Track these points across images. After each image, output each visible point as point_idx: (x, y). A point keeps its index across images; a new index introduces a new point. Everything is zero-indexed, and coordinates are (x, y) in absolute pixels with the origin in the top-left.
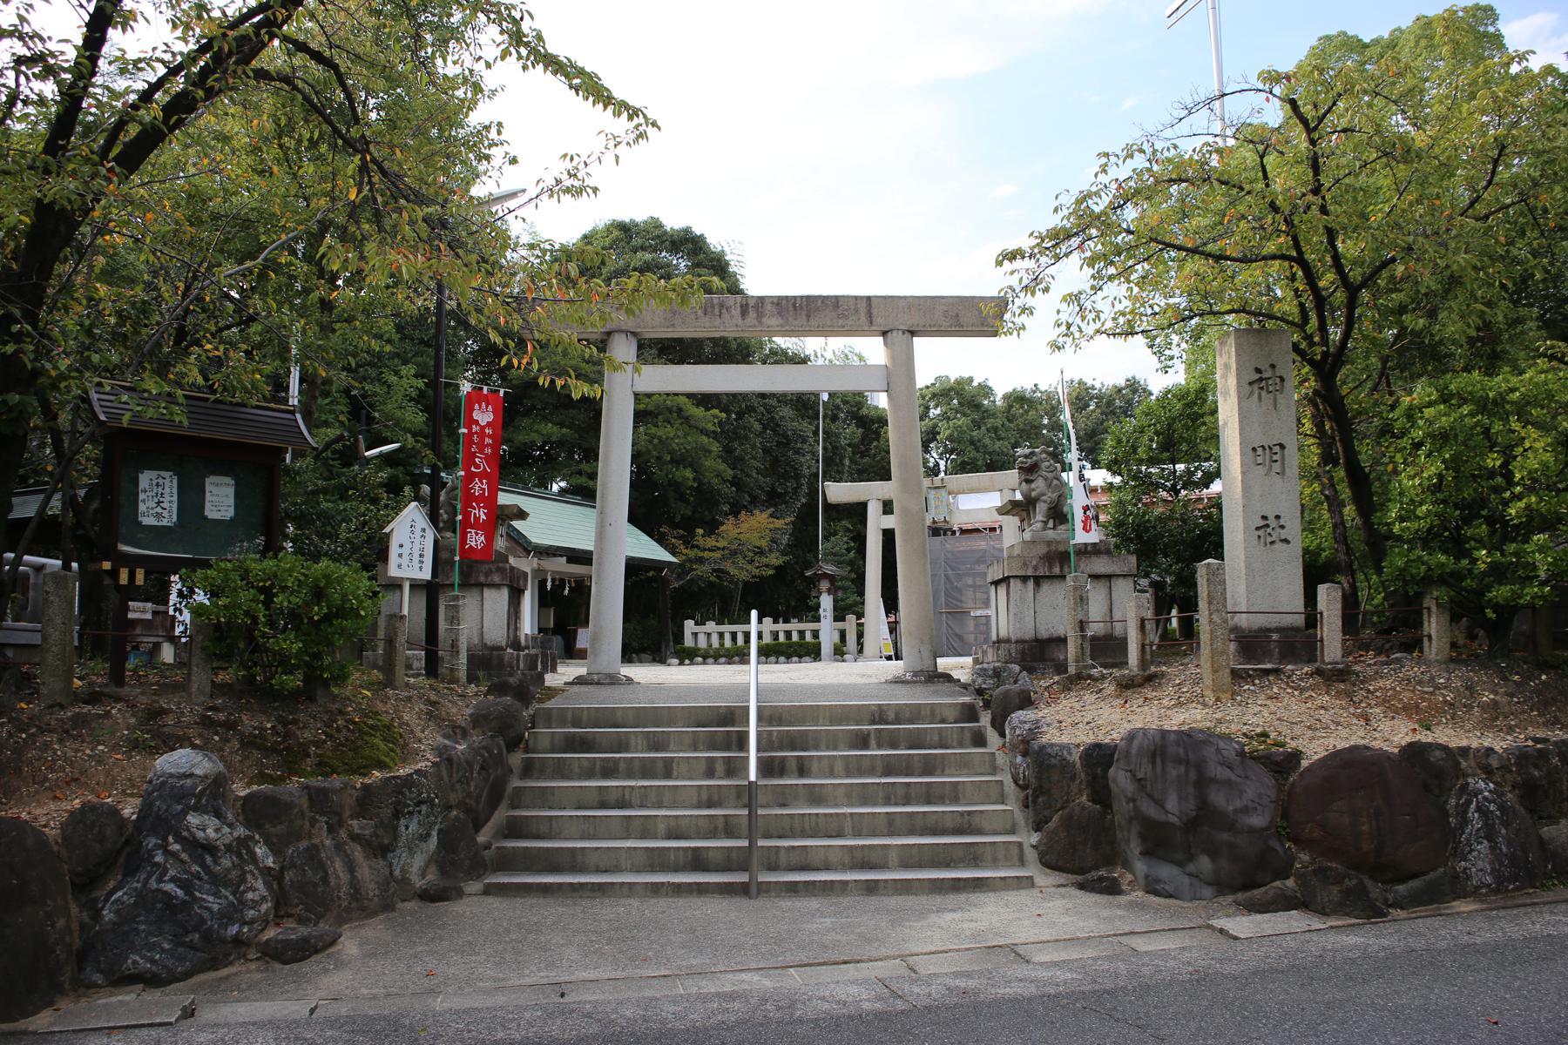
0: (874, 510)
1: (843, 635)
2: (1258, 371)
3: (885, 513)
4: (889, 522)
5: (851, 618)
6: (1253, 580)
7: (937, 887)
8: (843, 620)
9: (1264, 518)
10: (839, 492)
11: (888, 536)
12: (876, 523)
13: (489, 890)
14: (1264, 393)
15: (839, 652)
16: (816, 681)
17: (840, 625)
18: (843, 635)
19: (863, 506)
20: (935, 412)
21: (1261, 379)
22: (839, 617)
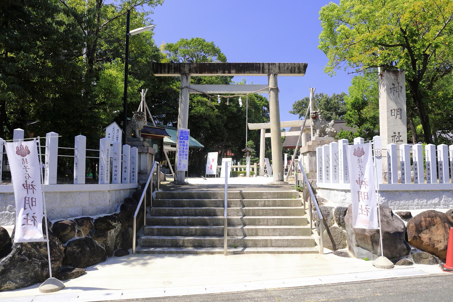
0: (262, 132)
1: (253, 169)
2: (393, 85)
3: (270, 132)
4: (268, 135)
5: (255, 164)
6: (162, 183)
7: (289, 244)
8: (253, 164)
9: (395, 133)
10: (252, 126)
11: (268, 140)
12: (263, 136)
13: (378, 208)
14: (395, 92)
15: (252, 174)
16: (366, 167)
17: (252, 166)
18: (253, 169)
19: (259, 131)
20: (224, 111)
21: (394, 88)
22: (252, 163)
